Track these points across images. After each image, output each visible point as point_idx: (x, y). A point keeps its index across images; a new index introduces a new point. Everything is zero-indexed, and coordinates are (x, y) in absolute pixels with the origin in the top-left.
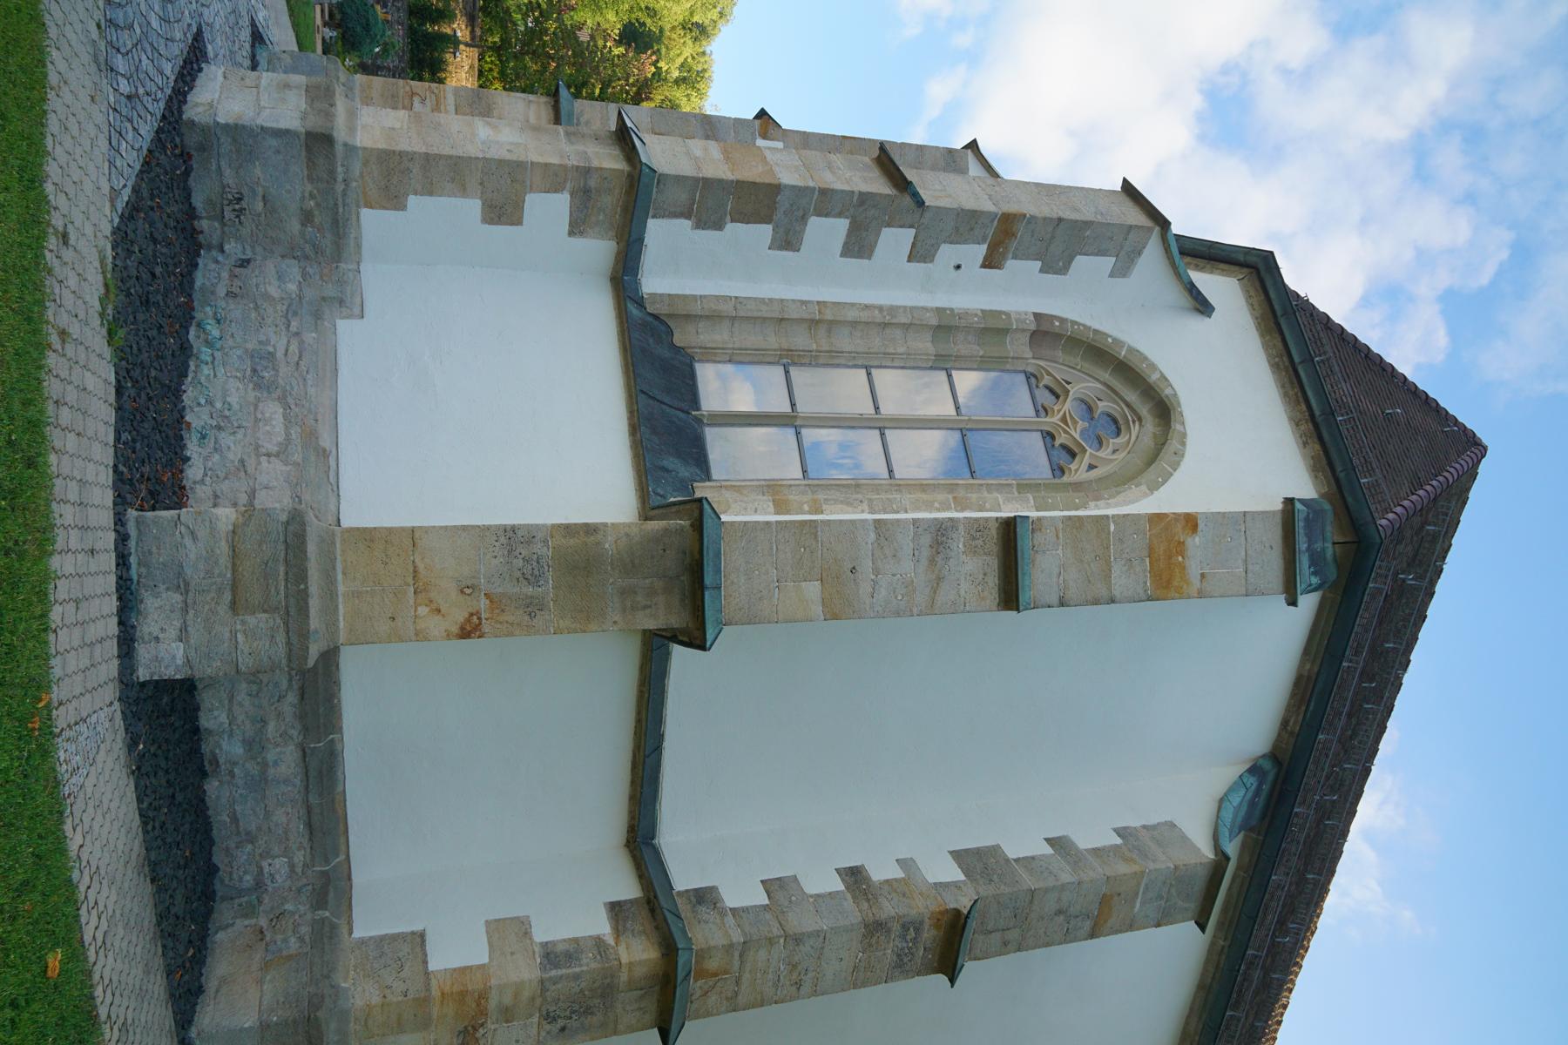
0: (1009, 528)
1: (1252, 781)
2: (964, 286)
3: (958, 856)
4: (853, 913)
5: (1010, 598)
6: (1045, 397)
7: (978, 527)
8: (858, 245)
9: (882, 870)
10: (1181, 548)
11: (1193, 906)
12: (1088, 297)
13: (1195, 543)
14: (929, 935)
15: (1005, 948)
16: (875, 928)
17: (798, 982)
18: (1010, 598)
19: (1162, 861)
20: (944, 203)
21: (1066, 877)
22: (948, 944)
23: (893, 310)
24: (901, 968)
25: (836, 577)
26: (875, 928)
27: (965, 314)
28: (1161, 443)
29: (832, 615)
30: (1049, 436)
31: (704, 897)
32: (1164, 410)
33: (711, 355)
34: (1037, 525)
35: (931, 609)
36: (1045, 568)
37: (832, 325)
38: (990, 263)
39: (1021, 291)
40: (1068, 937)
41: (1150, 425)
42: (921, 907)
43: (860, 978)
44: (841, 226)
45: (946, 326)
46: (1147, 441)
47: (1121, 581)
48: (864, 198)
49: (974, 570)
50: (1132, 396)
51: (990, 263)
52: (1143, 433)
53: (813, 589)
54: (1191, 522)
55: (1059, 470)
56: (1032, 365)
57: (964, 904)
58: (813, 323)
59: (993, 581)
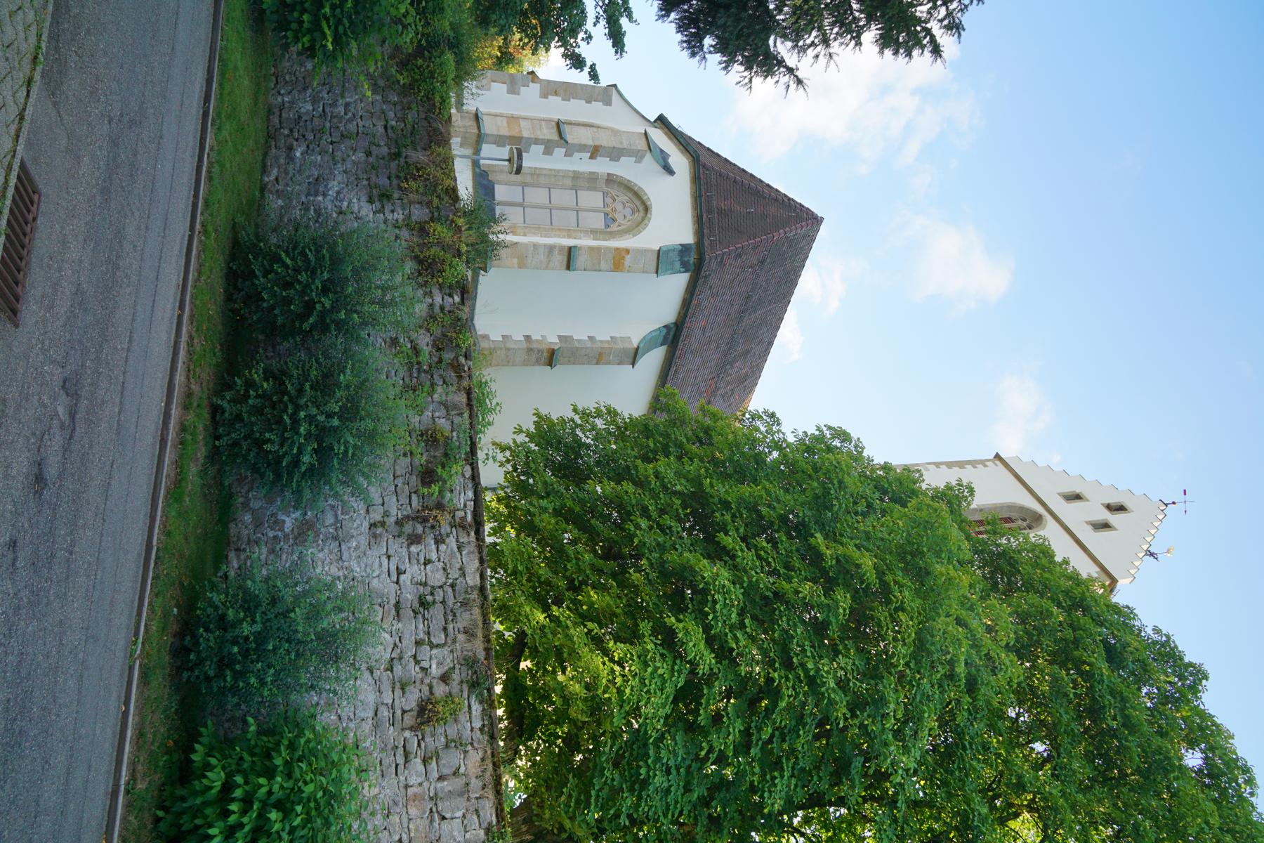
0: (570, 249)
1: (665, 331)
2: (583, 164)
3: (559, 337)
4: (525, 345)
5: (568, 268)
6: (609, 200)
7: (562, 248)
8: (548, 152)
9: (536, 337)
10: (623, 258)
11: (630, 360)
12: (625, 169)
13: (628, 258)
14: (545, 354)
15: (569, 363)
16: (530, 350)
17: (508, 361)
18: (568, 268)
19: (627, 346)
20: (576, 142)
21: (589, 345)
22: (551, 358)
23: (559, 171)
24: (538, 362)
25: (523, 257)
26: (530, 350)
27: (583, 173)
28: (643, 219)
29: (520, 267)
30: (606, 214)
31: (485, 337)
32: (647, 209)
33: (499, 183)
34: (580, 248)
35: (546, 268)
36: (581, 260)
37: (538, 175)
38: (591, 158)
39: (602, 166)
40: (589, 363)
41: (642, 214)
42: (544, 346)
43: (526, 363)
44: (542, 147)
45: (576, 176)
46: (640, 219)
47: (603, 265)
48: (549, 141)
49: (560, 259)
50: (638, 203)
51: (591, 158)
52: (638, 216)
53: (515, 260)
54: (627, 251)
55: (607, 226)
56: (605, 189)
57: (556, 347)
58: (532, 175)
59: (565, 263)
